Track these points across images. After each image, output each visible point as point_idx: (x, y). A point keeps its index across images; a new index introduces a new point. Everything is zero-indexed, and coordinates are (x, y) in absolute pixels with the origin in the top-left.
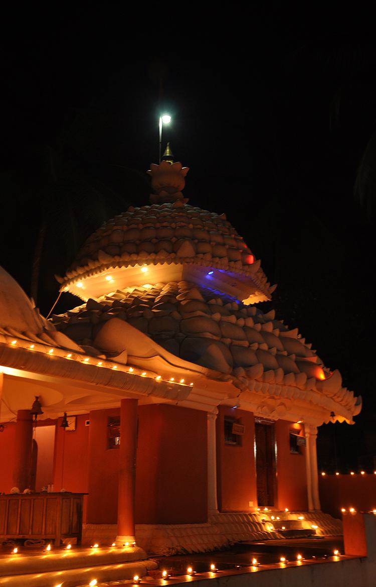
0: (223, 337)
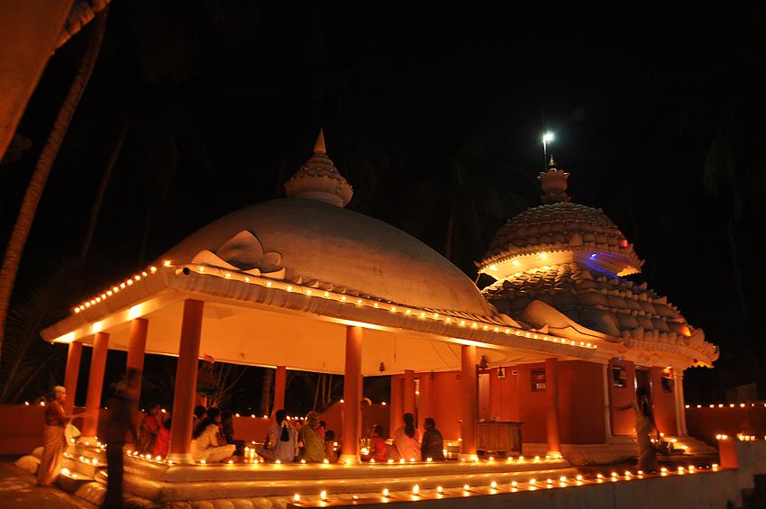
0: (611, 307)
